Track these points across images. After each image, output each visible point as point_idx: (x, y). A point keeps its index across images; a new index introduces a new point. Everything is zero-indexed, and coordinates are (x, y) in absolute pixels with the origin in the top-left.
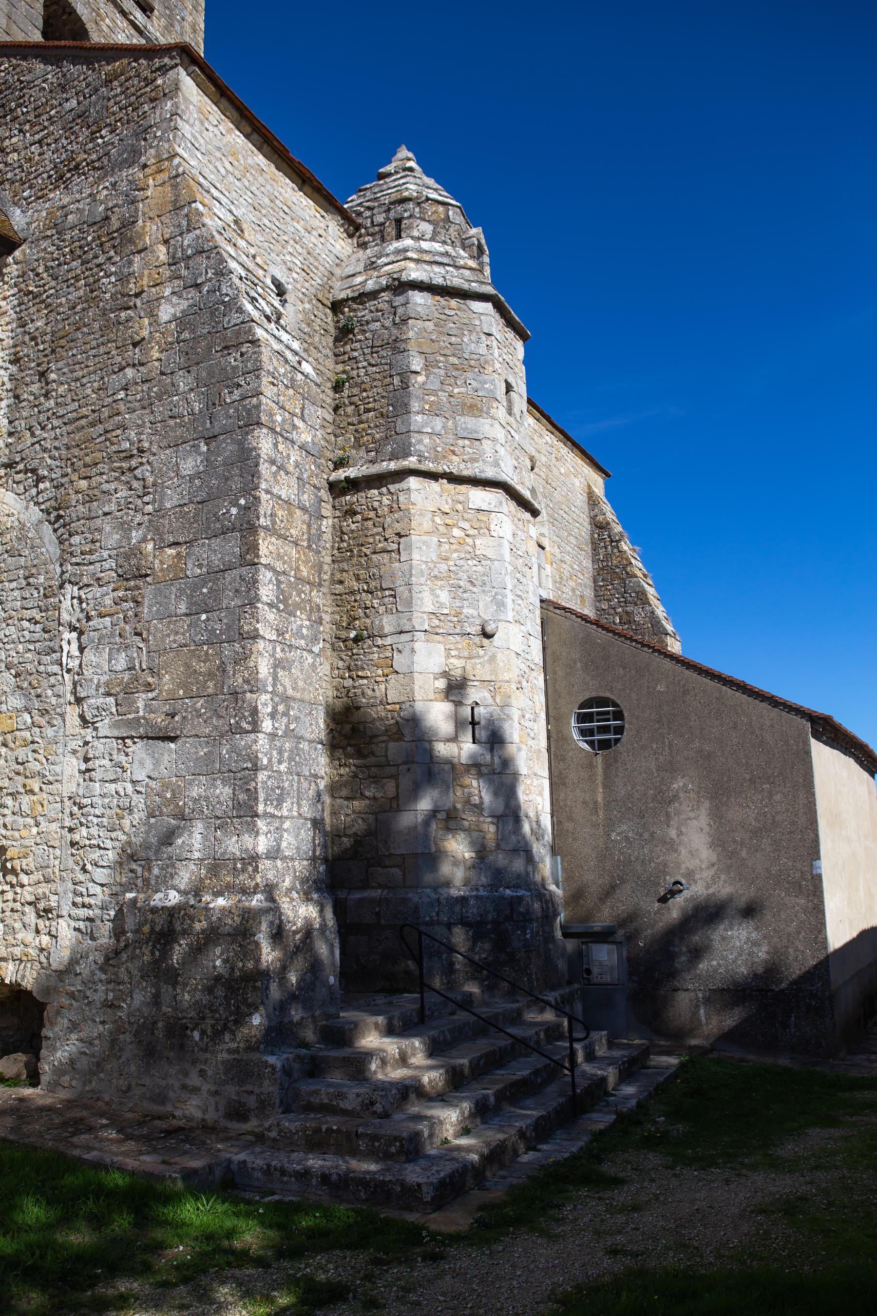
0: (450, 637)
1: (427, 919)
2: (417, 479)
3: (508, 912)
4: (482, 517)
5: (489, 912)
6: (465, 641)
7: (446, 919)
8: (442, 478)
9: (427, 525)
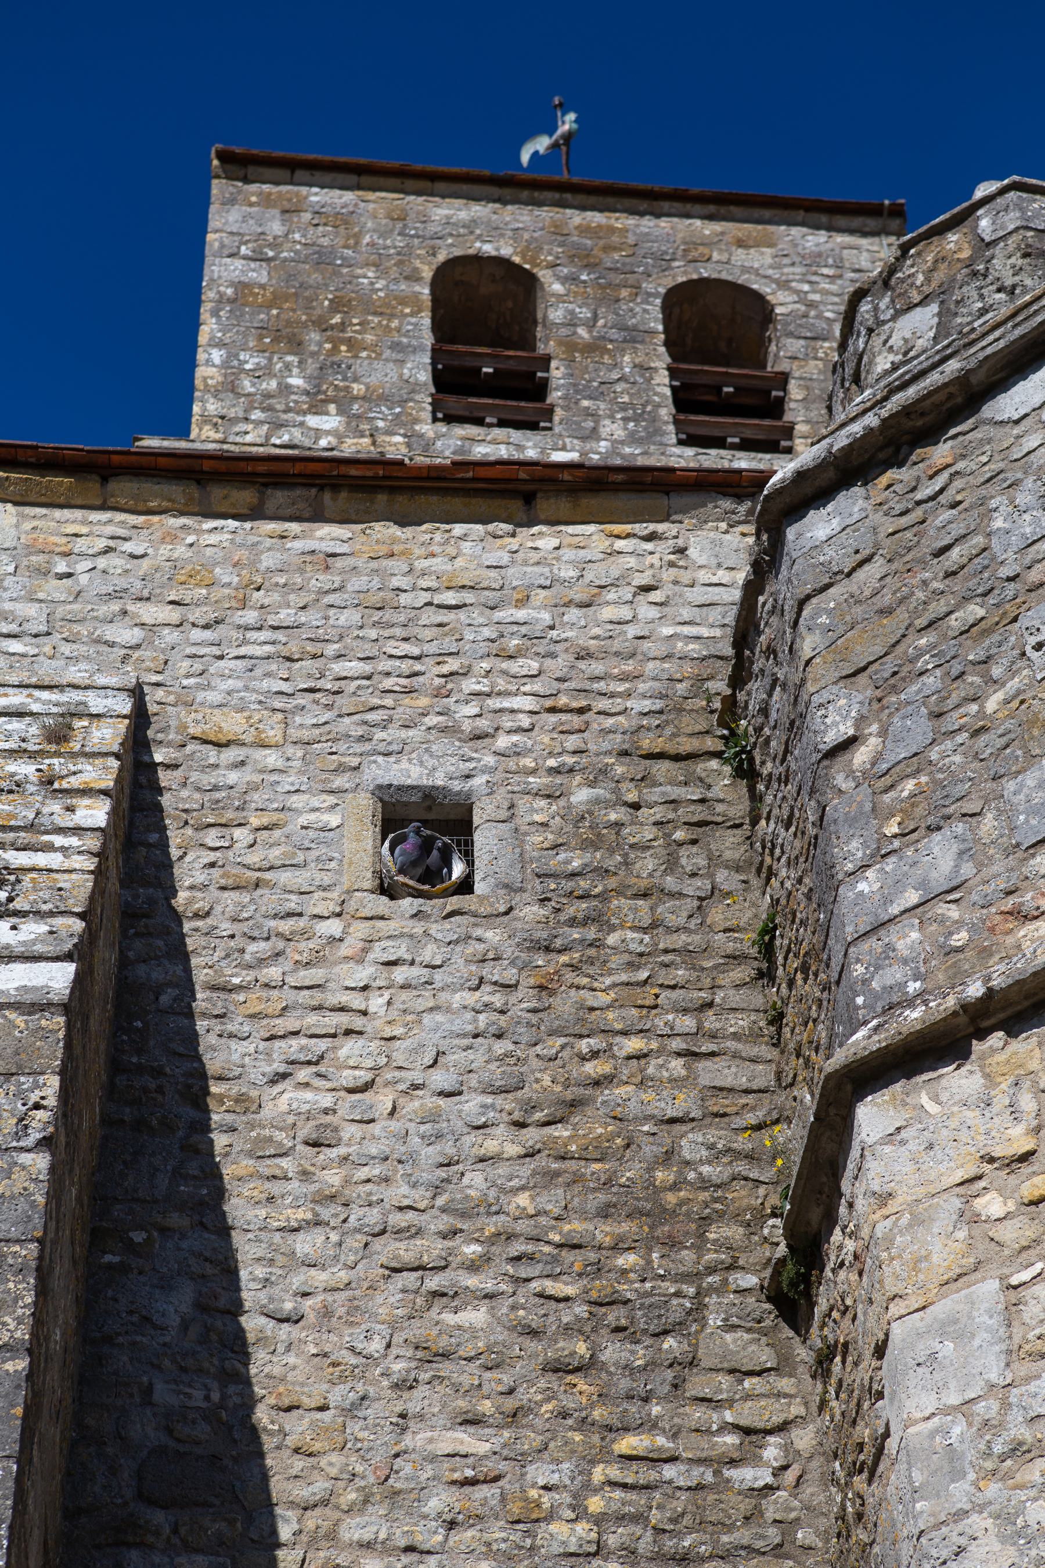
2: (883, 1096)
8: (982, 1034)
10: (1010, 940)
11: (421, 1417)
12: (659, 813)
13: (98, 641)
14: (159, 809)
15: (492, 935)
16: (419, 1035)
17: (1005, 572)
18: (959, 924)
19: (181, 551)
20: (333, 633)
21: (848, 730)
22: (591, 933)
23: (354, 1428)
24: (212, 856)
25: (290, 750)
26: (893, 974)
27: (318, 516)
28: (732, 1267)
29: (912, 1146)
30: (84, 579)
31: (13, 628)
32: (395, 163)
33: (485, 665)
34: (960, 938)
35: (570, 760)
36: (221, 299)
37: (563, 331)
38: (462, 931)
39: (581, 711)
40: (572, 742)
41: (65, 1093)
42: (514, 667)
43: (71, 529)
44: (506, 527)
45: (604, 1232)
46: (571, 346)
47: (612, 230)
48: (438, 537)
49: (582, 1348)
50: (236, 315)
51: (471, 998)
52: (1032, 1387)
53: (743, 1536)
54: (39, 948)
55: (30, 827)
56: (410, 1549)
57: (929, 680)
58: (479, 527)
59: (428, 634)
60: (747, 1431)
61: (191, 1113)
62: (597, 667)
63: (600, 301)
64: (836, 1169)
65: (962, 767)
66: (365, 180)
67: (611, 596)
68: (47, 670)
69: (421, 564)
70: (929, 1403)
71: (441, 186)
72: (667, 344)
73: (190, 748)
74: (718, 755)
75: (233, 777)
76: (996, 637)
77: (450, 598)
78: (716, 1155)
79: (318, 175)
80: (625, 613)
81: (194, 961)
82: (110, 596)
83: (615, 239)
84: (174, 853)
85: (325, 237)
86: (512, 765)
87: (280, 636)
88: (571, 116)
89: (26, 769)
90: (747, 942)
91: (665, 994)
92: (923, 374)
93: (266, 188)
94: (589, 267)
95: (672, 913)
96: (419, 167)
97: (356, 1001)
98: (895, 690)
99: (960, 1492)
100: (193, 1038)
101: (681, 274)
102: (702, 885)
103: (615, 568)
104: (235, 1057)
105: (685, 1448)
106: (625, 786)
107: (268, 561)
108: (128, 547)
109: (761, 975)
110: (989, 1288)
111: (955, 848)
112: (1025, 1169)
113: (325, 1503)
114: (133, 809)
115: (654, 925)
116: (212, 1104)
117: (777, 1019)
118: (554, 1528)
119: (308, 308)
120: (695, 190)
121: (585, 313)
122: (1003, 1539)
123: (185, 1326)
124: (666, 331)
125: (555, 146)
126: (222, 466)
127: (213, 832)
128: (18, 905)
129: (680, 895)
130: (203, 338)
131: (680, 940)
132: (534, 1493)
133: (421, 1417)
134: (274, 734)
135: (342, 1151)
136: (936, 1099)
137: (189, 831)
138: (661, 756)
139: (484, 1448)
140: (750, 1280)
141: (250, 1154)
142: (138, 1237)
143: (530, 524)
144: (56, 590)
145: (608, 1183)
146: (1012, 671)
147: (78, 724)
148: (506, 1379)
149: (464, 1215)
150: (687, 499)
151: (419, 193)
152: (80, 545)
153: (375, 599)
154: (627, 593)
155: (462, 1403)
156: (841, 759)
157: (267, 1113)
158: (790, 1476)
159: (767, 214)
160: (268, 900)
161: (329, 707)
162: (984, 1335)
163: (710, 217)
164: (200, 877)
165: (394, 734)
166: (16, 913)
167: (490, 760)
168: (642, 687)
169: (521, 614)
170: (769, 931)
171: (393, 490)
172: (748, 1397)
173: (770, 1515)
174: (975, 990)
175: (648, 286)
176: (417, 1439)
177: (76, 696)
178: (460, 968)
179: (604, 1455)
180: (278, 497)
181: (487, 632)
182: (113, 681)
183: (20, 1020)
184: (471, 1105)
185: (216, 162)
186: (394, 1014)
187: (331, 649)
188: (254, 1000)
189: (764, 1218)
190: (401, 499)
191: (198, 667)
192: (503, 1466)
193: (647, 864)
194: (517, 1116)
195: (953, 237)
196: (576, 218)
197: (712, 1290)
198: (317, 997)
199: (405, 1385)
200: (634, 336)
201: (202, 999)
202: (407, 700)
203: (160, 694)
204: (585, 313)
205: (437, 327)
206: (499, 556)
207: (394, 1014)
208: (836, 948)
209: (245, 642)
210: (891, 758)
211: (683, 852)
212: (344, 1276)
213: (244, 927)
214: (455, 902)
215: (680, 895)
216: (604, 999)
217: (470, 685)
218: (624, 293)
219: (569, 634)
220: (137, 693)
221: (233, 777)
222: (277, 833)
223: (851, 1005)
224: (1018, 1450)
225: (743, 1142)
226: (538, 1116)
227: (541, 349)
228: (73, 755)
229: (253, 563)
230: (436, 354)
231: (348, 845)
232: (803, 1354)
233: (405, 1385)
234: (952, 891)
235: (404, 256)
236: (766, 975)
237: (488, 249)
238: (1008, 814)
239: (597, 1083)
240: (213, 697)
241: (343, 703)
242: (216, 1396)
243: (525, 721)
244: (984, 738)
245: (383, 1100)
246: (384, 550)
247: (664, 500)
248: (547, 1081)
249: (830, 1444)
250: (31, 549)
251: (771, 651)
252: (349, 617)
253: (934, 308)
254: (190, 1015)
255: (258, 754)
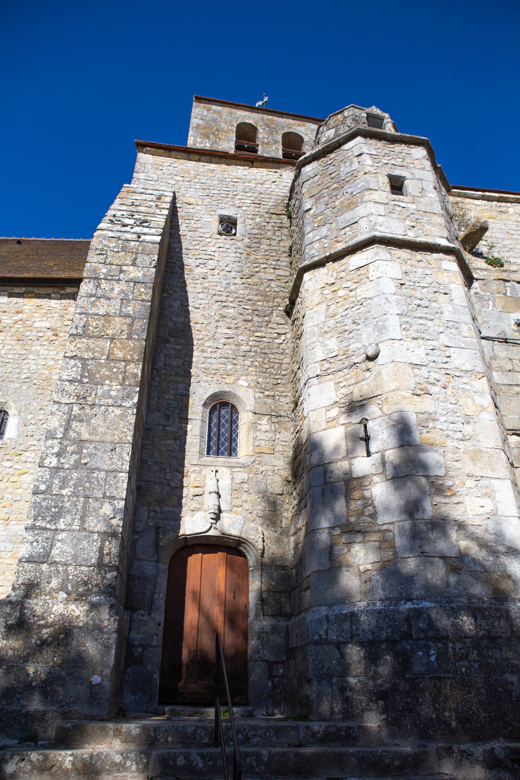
0: (339, 373)
1: (316, 637)
3: (405, 628)
4: (362, 271)
5: (381, 629)
6: (353, 372)
7: (335, 638)
8: (328, 262)
9: (317, 299)
10: (335, 246)
11: (220, 327)
12: (273, 224)
13: (167, 183)
14: (177, 215)
15: (239, 244)
16: (224, 261)
17: (342, 178)
18: (326, 243)
19: (184, 167)
20: (212, 185)
21: (310, 207)
22: (258, 245)
23: (208, 327)
24: (187, 225)
25: (203, 206)
26: (313, 251)
27: (211, 162)
28: (279, 306)
29: (313, 281)
30: (165, 171)
31: (151, 179)
32: (230, 102)
33: (242, 194)
34: (326, 245)
35: (256, 213)
36: (194, 127)
37: (262, 140)
38: (233, 243)
39: (259, 204)
40: (257, 210)
41: (158, 259)
42: (247, 194)
43: (163, 161)
44: (247, 168)
45: (256, 298)
46: (263, 143)
47: (273, 120)
48: (234, 168)
49: (250, 318)
50: (196, 130)
51: (234, 255)
52: (329, 322)
53: (276, 351)
54: (154, 233)
55: (153, 213)
56: (217, 348)
57: (326, 198)
58: (242, 167)
59: (231, 187)
60: (279, 334)
61: (180, 271)
62: (263, 196)
63: (270, 134)
64: (299, 287)
65: (330, 214)
66: (224, 105)
67: (267, 183)
68: (157, 187)
69: (230, 173)
70: (311, 324)
71: (239, 107)
72: (282, 144)
73: (184, 204)
74: (284, 214)
75: (192, 211)
76: (339, 191)
77: (236, 180)
78: (278, 286)
79: (215, 103)
80: (269, 186)
81: (183, 244)
82: (170, 174)
83: (274, 122)
84: (180, 224)
85: (215, 116)
86: (245, 213)
87: (202, 185)
88: (267, 98)
89: (152, 204)
90: (287, 249)
91: (271, 257)
92: (331, 141)
93: (204, 105)
94: (268, 127)
95: (274, 243)
96: (235, 103)
97: (213, 254)
98: (319, 200)
99: (315, 339)
100: (182, 258)
101: (286, 130)
102: (280, 238)
103: (268, 177)
104: (190, 262)
105: (267, 336)
106: (266, 219)
107: (201, 170)
108: (174, 165)
109: (289, 255)
110: (324, 306)
111: (327, 229)
112: (333, 286)
113: (202, 339)
114: (172, 215)
115: (270, 245)
116: (185, 270)
117: (291, 263)
118: (243, 347)
119: (211, 130)
120: (290, 113)
121: (266, 136)
122: (321, 346)
123: (178, 308)
124: (282, 142)
125: (263, 104)
126: (193, 151)
127: (187, 221)
128: (150, 226)
129: (275, 240)
130: (189, 135)
131: (274, 248)
132: (239, 341)
133: (220, 327)
134: (200, 203)
135: (208, 280)
136: (318, 273)
137: (183, 220)
138: (274, 214)
139: (231, 333)
140: (282, 309)
141: (191, 279)
142: (170, 292)
143: (252, 167)
144: (159, 172)
145: (257, 290)
146: (341, 197)
147: (163, 197)
148: (236, 322)
149: (230, 293)
150: (283, 165)
151: (235, 108)
152: (164, 164)
153: (221, 179)
154: (270, 183)
155: (228, 325)
156: (308, 213)
157: (195, 272)
158: (285, 342)
159: (304, 120)
160: (197, 234)
161: (211, 199)
162: (322, 313)
163: (293, 119)
164: (185, 229)
165: (223, 205)
166: (150, 227)
167: (241, 212)
168: (271, 200)
169: (249, 185)
170: (291, 247)
171: (226, 158)
172: (279, 328)
173: (281, 348)
174: (328, 254)
175: (279, 132)
176: (219, 330)
177: (163, 192)
178: (233, 249)
179: (253, 336)
180: (203, 158)
181: (242, 187)
182: (170, 190)
183: (151, 245)
184: (233, 274)
185: (194, 99)
186: (220, 256)
187: (212, 188)
188: (194, 252)
189: (285, 298)
190: (227, 160)
191: (186, 189)
192: (234, 336)
193: (269, 234)
194: (241, 277)
195: (339, 116)
196: (266, 117)
197: (274, 310)
198: (205, 252)
199: (218, 321)
200: (276, 142)
201: (184, 251)
202: (226, 199)
203: (178, 194)
204: (266, 136)
205: (237, 137)
206: (246, 173)
207: (220, 256)
208: (303, 247)
209: (195, 185)
210: (317, 212)
211: (277, 232)
212: (208, 302)
213: (192, 238)
214: (232, 237)
215: (275, 240)
216: (259, 257)
217: (238, 197)
218: (275, 133)
219: (258, 189)
220: (174, 193)
221: (192, 211)
222: (199, 222)
223: (305, 257)
224: (326, 332)
225: (282, 285)
226: (245, 277)
227: (257, 143)
228: (162, 202)
229: (198, 170)
230: (236, 141)
231: (213, 225)
232: (290, 322)
233: (218, 321)
234: (326, 237)
235: (231, 121)
236: (290, 256)
237: (248, 121)
238: (337, 223)
239: (257, 272)
240: (189, 195)
241: (214, 198)
242: (183, 320)
243: (248, 205)
244: (334, 209)
245: (216, 272)
246: (223, 170)
247: (279, 165)
248: (247, 271)
249: (293, 336)
250: (155, 164)
251: (297, 193)
252: (216, 182)
253: (334, 129)
254: (181, 253)
255: (197, 207)
